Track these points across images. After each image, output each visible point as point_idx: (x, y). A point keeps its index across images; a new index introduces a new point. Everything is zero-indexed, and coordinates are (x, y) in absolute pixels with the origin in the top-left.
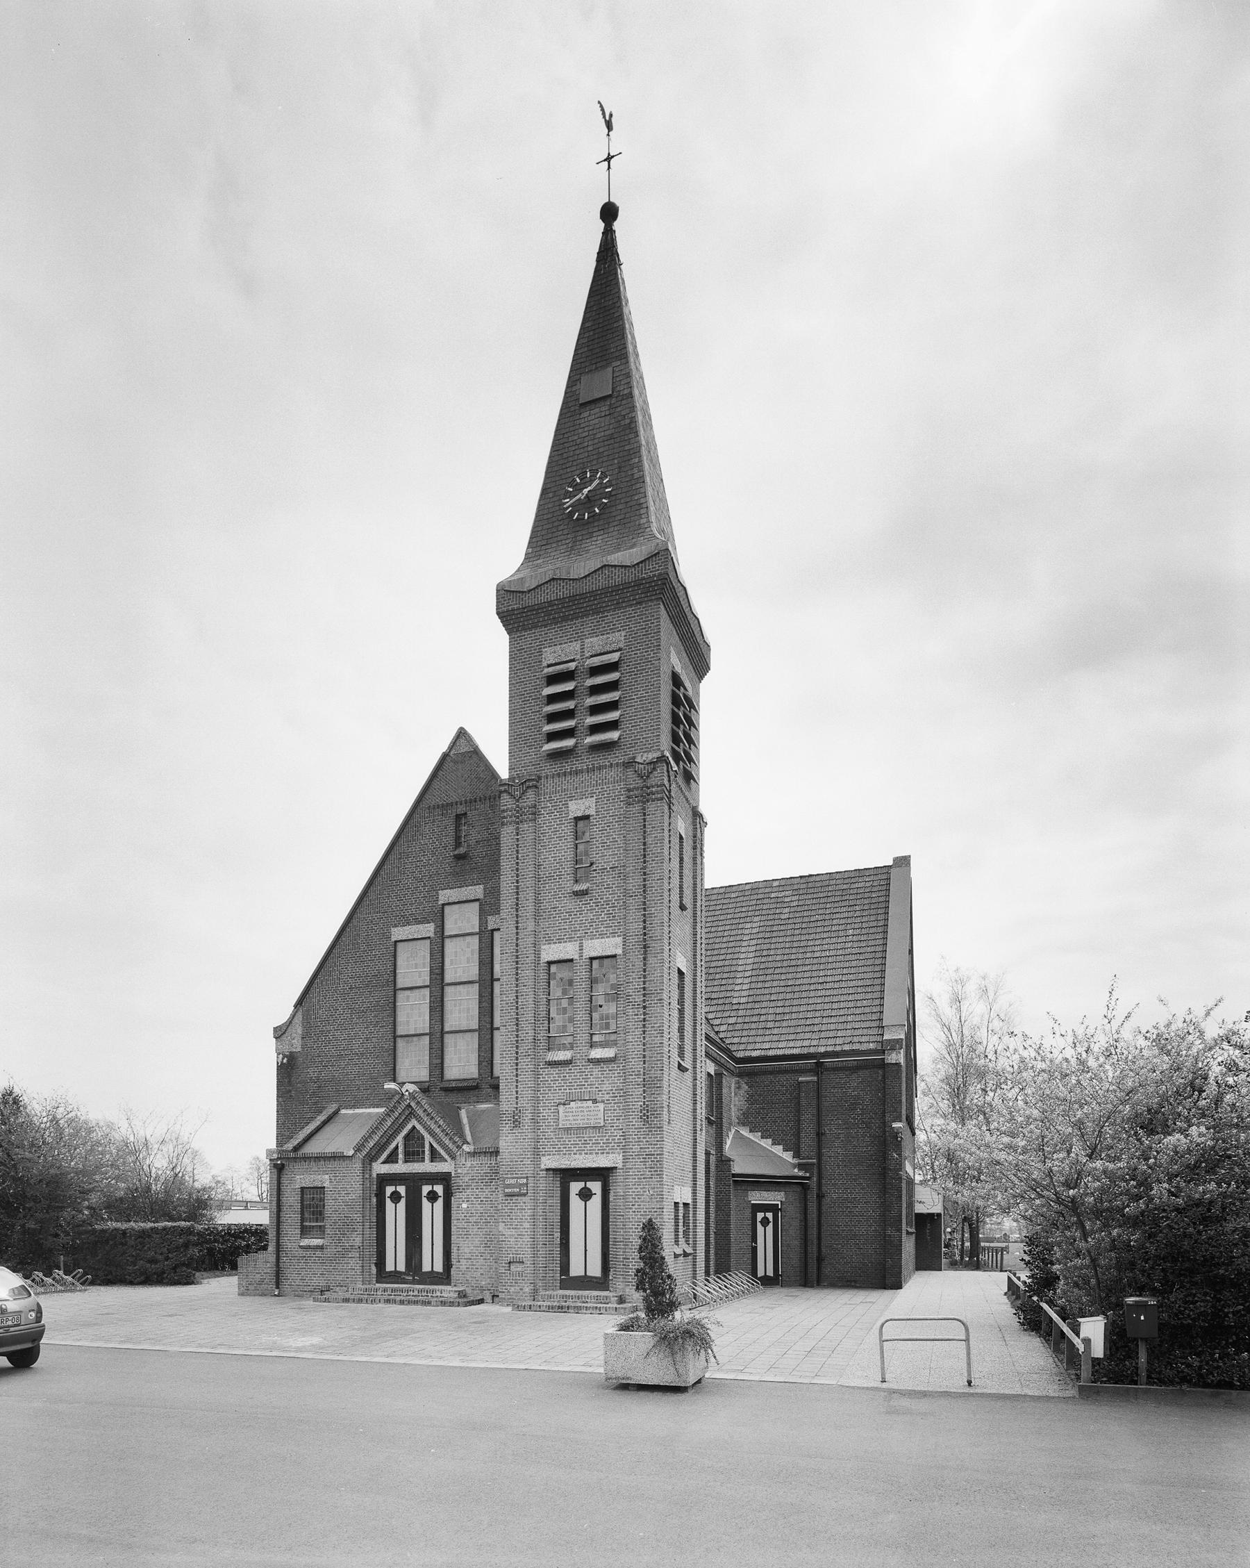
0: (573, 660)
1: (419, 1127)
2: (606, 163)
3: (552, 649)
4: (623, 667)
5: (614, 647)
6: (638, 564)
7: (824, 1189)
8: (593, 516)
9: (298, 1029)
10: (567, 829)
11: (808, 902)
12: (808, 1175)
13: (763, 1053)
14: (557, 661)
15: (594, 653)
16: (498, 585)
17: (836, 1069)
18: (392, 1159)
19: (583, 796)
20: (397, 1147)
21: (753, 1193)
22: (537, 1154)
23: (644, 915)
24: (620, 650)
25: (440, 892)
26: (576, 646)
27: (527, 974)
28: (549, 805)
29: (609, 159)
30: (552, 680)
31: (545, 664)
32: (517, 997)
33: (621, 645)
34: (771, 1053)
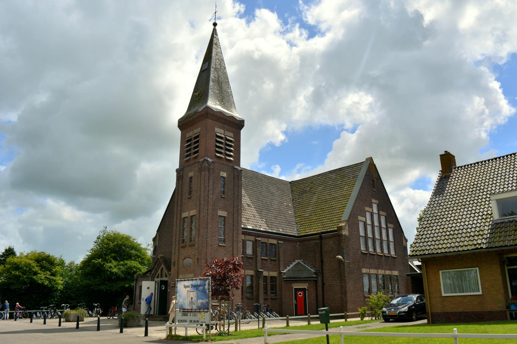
7: (325, 282)
13: (326, 230)
14: (189, 136)
17: (326, 238)
18: (158, 277)
20: (159, 274)
21: (294, 284)
26: (192, 132)
29: (215, 13)
30: (188, 141)
31: (187, 138)
34: (309, 233)
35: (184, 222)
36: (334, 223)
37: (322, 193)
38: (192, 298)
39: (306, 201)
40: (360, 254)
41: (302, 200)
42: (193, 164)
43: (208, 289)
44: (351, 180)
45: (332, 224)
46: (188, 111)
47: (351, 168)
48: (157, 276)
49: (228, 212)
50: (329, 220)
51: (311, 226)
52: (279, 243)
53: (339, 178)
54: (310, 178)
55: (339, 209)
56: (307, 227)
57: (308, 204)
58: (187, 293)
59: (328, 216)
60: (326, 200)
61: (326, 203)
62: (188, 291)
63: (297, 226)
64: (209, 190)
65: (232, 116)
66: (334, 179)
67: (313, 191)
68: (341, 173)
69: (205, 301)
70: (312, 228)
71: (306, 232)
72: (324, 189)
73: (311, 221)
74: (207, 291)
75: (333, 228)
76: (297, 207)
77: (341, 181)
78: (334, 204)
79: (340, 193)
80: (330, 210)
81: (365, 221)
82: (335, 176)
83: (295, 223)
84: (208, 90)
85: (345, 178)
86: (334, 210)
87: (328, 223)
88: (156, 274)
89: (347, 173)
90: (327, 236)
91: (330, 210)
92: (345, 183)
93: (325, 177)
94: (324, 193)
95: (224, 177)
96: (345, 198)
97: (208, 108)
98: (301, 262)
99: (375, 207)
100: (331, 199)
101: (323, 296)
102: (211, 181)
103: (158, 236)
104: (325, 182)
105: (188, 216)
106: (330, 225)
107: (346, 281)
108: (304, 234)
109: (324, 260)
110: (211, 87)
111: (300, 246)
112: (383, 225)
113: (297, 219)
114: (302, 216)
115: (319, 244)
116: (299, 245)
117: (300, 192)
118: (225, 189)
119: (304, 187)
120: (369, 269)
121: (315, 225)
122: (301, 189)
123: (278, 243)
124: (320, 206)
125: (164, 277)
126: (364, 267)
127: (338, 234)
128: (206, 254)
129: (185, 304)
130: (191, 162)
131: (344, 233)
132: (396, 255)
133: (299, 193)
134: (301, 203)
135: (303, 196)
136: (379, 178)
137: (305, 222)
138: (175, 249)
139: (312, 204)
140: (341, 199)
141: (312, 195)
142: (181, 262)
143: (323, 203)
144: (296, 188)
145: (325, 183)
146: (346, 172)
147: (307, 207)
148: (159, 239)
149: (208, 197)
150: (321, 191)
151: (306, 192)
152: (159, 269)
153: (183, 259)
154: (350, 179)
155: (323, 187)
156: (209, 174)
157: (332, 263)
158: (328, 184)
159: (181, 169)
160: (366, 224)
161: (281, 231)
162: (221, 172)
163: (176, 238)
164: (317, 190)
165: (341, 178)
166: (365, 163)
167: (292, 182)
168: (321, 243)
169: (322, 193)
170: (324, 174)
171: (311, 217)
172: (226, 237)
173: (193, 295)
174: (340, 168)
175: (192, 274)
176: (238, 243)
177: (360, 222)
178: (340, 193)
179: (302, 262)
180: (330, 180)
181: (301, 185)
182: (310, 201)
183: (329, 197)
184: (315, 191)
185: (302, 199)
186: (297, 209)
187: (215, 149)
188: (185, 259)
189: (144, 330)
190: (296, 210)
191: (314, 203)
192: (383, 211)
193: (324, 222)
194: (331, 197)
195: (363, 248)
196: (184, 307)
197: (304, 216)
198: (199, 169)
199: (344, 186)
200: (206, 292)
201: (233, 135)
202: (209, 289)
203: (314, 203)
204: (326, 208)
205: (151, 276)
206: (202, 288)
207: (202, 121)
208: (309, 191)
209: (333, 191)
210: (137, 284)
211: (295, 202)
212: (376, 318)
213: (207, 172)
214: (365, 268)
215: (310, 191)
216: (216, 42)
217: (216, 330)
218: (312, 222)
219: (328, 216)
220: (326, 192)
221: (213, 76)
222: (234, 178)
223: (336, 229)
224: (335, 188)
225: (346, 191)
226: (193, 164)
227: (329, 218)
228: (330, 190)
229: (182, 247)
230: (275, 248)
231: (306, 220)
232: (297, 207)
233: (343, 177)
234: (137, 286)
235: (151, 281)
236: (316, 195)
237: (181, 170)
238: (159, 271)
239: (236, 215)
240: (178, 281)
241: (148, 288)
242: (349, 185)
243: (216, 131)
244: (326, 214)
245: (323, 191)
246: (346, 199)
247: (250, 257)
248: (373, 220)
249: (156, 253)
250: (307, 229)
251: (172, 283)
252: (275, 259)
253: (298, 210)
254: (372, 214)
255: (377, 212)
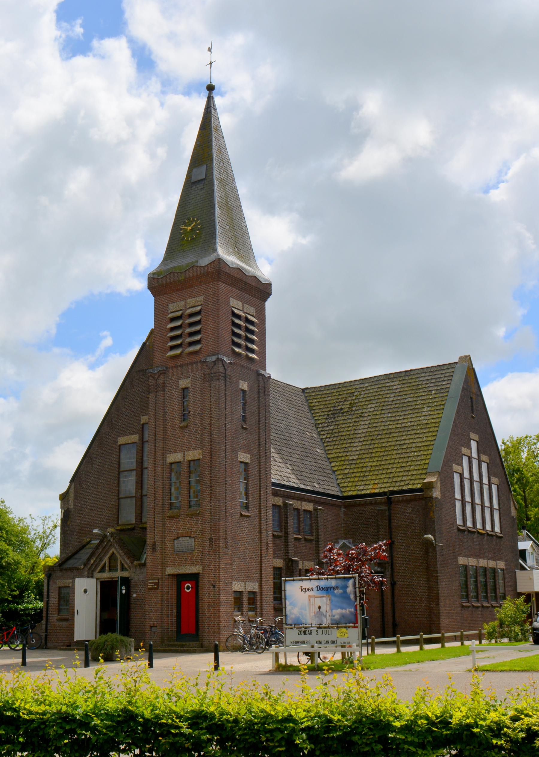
0: (181, 310)
1: (115, 552)
2: (210, 65)
3: (172, 305)
4: (203, 313)
5: (199, 303)
6: (207, 265)
7: (396, 579)
8: (193, 239)
9: (72, 495)
10: (178, 394)
11: (406, 389)
12: (383, 570)
13: (400, 488)
14: (175, 310)
15: (190, 306)
16: (148, 275)
17: (398, 502)
18: (102, 570)
19: (185, 378)
20: (105, 564)
22: (163, 567)
23: (211, 438)
24: (201, 305)
25: (141, 417)
26: (183, 303)
27: (159, 470)
28: (171, 382)
29: (211, 63)
30: (173, 320)
31: (169, 312)
32: (155, 482)
33: (202, 303)
34: (364, 492)
35: (171, 470)
36: (413, 475)
37: (377, 417)
38: (320, 608)
39: (346, 429)
40: (456, 531)
41: (336, 427)
42: (188, 364)
43: (352, 593)
44: (433, 396)
45: (409, 478)
46: (166, 259)
47: (430, 372)
48: (99, 568)
49: (252, 455)
50: (402, 470)
51: (365, 479)
52: (318, 509)
53: (408, 390)
54: (346, 384)
55: (417, 449)
56: (356, 479)
57: (351, 437)
58: (309, 600)
59: (397, 461)
60: (389, 431)
61: (389, 438)
62: (309, 596)
63: (337, 477)
64: (226, 414)
65: (255, 276)
66: (398, 390)
67: (357, 412)
68: (410, 381)
69: (348, 612)
70: (368, 482)
71: (358, 490)
72: (380, 408)
73: (364, 469)
74: (352, 596)
75: (413, 484)
76: (327, 440)
77: (413, 397)
78: (405, 439)
79: (415, 419)
80: (400, 451)
81: (461, 472)
82: (399, 384)
83: (330, 472)
84: (215, 224)
85: (421, 392)
86: (408, 451)
87: (401, 474)
88: (97, 566)
89: (424, 383)
90: (401, 499)
91: (400, 451)
92: (421, 400)
93: (378, 386)
94: (381, 416)
95: (244, 391)
96: (427, 430)
97: (219, 261)
98: (349, 545)
99: (474, 445)
100: (398, 430)
101: (393, 604)
102: (229, 399)
103: (72, 490)
104: (379, 395)
105: (182, 460)
106: (404, 478)
107: (439, 578)
108: (355, 493)
109: (394, 541)
110: (219, 219)
111: (345, 514)
112: (485, 480)
113: (333, 464)
114: (343, 458)
115: (387, 513)
116: (344, 512)
117: (330, 411)
118: (247, 412)
119: (335, 401)
120: (467, 558)
121: (374, 477)
122: (330, 406)
123: (316, 510)
124: (377, 441)
125: (107, 571)
126: (460, 555)
127: (425, 496)
128: (226, 531)
129: (304, 616)
130: (182, 361)
131: (434, 495)
132: (501, 533)
133: (326, 413)
134: (335, 433)
135: (336, 419)
136: (479, 393)
137: (351, 471)
138: (154, 521)
139: (361, 437)
140: (420, 431)
141: (357, 420)
142: (169, 544)
143: (383, 436)
144: (319, 402)
145: (380, 397)
146: (421, 379)
147: (349, 441)
148: (76, 498)
149: (226, 427)
150: (375, 413)
151: (343, 413)
152: (105, 555)
153: (174, 540)
154: (431, 395)
155: (378, 405)
156: (225, 386)
157: (412, 548)
158: (387, 399)
159: (160, 372)
160: (462, 476)
161: (317, 487)
162: (240, 381)
163: (155, 500)
164: (365, 410)
165: (412, 390)
166: (458, 365)
167: (306, 389)
168: (389, 510)
169: (377, 417)
170: (376, 379)
171: (362, 461)
172: (250, 499)
173: (324, 602)
174: (406, 371)
175: (197, 566)
176: (267, 510)
177: (455, 474)
178: (415, 419)
179: (350, 543)
180: (389, 392)
181: (329, 398)
182: (355, 430)
183: (394, 426)
184: (360, 411)
185: (335, 425)
186: (329, 444)
187: (232, 338)
188: (178, 538)
189: (213, 657)
190: (327, 446)
191: (363, 435)
192: (484, 453)
193: (391, 473)
194: (399, 426)
195: (459, 522)
196: (303, 620)
197: (347, 458)
198: (205, 375)
199: (420, 406)
200: (349, 598)
201: (255, 312)
202: (355, 592)
203: (363, 435)
204: (390, 446)
205: (86, 569)
206: (341, 591)
207: (206, 284)
208: (348, 411)
209: (398, 414)
210: (51, 583)
211: (322, 431)
212: (496, 642)
213: (222, 383)
214: (463, 557)
215: (352, 411)
216: (216, 126)
217: (308, 660)
218: (366, 471)
219: (397, 461)
220: (386, 416)
221: (219, 195)
222: (259, 392)
223: (419, 486)
224: (404, 409)
225: (427, 417)
226: (188, 364)
227: (399, 465)
228: (393, 412)
229: (171, 517)
230: (311, 518)
231: (353, 466)
232: (327, 440)
233: (416, 389)
234: (50, 588)
235: (88, 577)
236: (365, 419)
237: (160, 374)
238: (106, 560)
239: (263, 460)
240: (286, 581)
241: (85, 591)
242: (431, 404)
243: (231, 305)
244: (393, 457)
245: (379, 413)
246: (429, 432)
247: (278, 535)
248: (472, 470)
249: (68, 523)
250: (359, 483)
251: (151, 581)
252: (312, 538)
253: (331, 445)
254: (470, 459)
255: (477, 457)
